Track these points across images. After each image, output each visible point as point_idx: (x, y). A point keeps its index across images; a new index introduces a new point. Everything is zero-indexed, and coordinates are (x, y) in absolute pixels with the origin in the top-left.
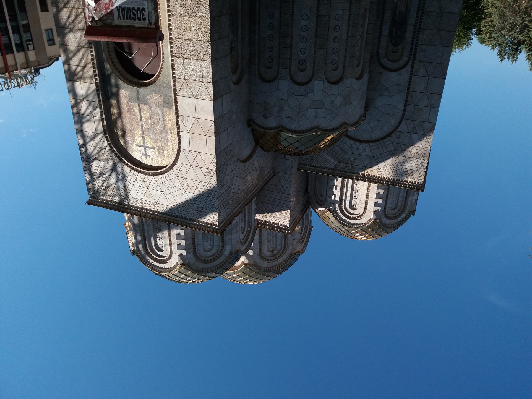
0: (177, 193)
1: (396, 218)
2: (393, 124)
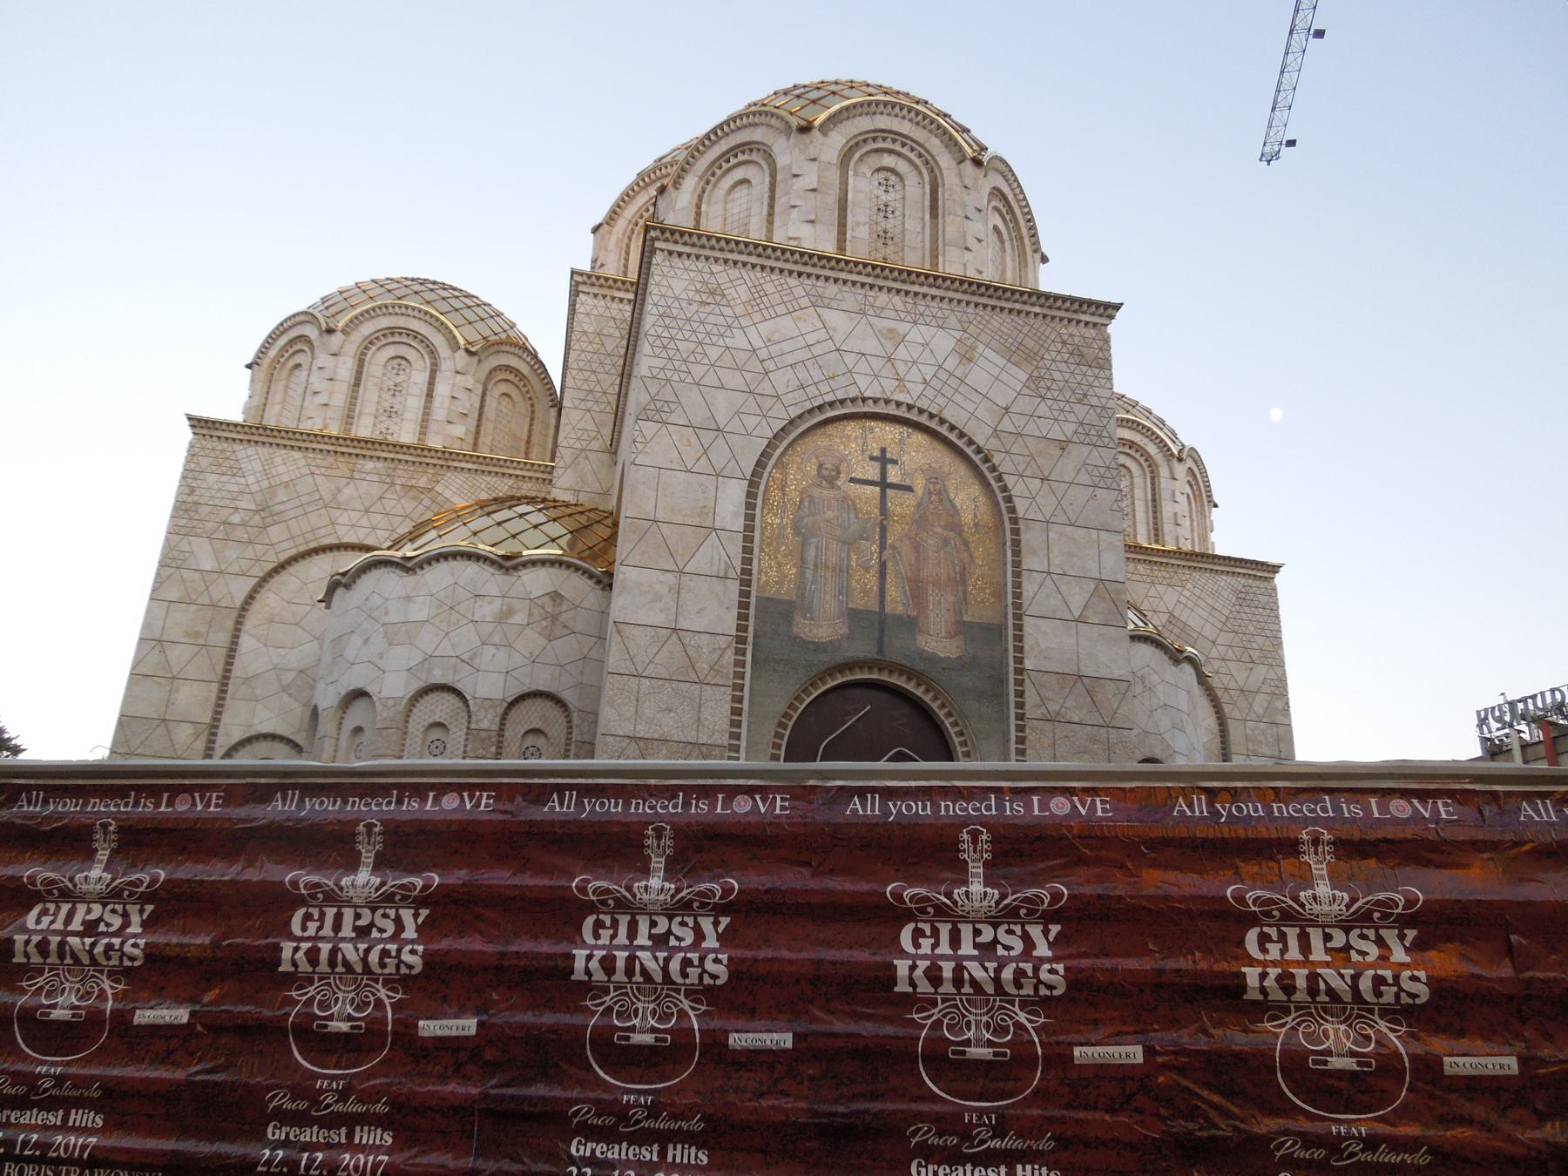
0: (786, 346)
1: (291, 342)
2: (271, 595)
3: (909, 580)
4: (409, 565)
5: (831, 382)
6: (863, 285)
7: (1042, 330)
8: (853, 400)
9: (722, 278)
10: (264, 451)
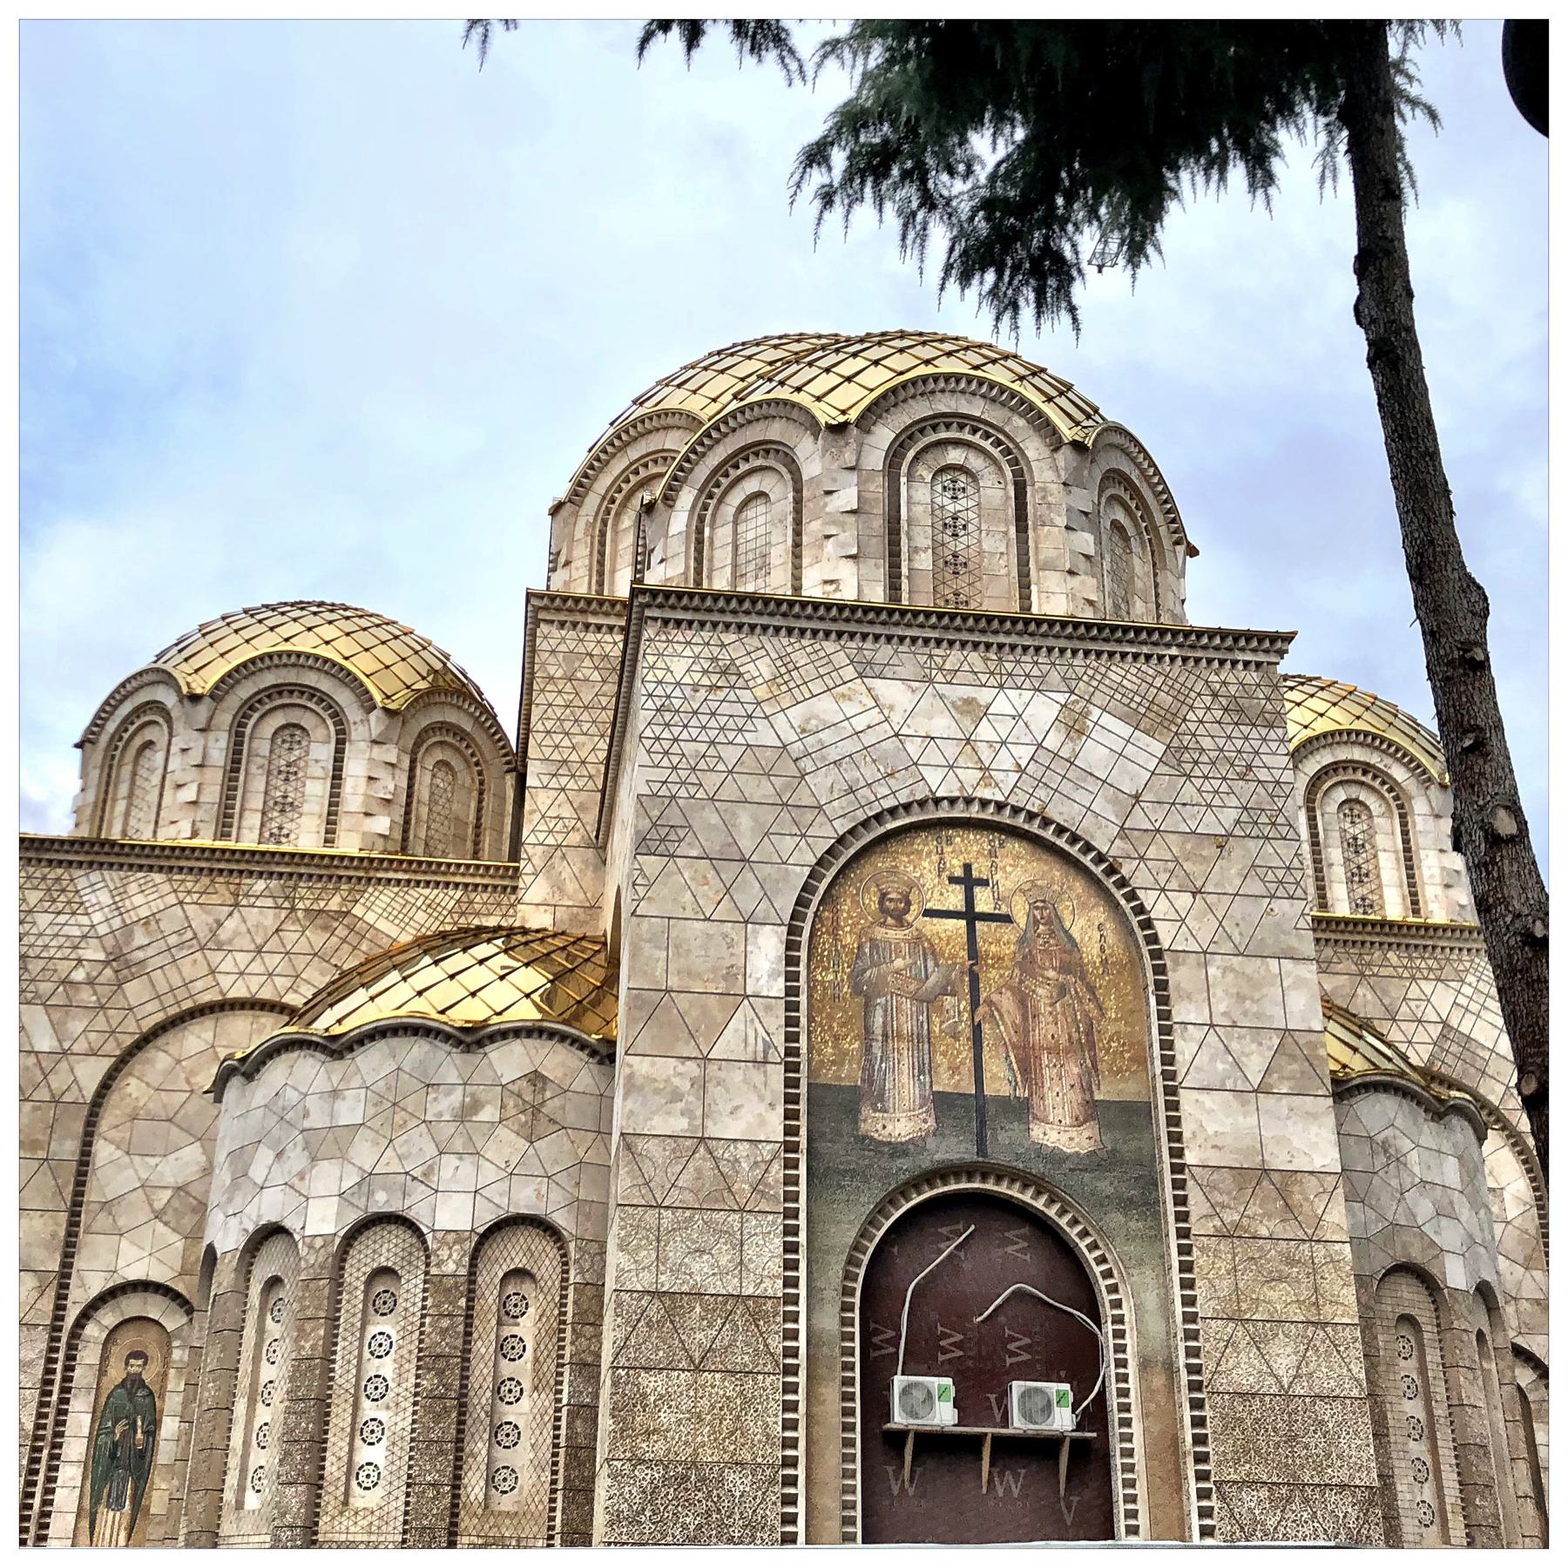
0: (826, 736)
1: (138, 711)
3: (1014, 1047)
4: (334, 1047)
5: (891, 781)
6: (926, 641)
7: (1182, 680)
8: (922, 803)
9: (736, 652)
10: (112, 877)
